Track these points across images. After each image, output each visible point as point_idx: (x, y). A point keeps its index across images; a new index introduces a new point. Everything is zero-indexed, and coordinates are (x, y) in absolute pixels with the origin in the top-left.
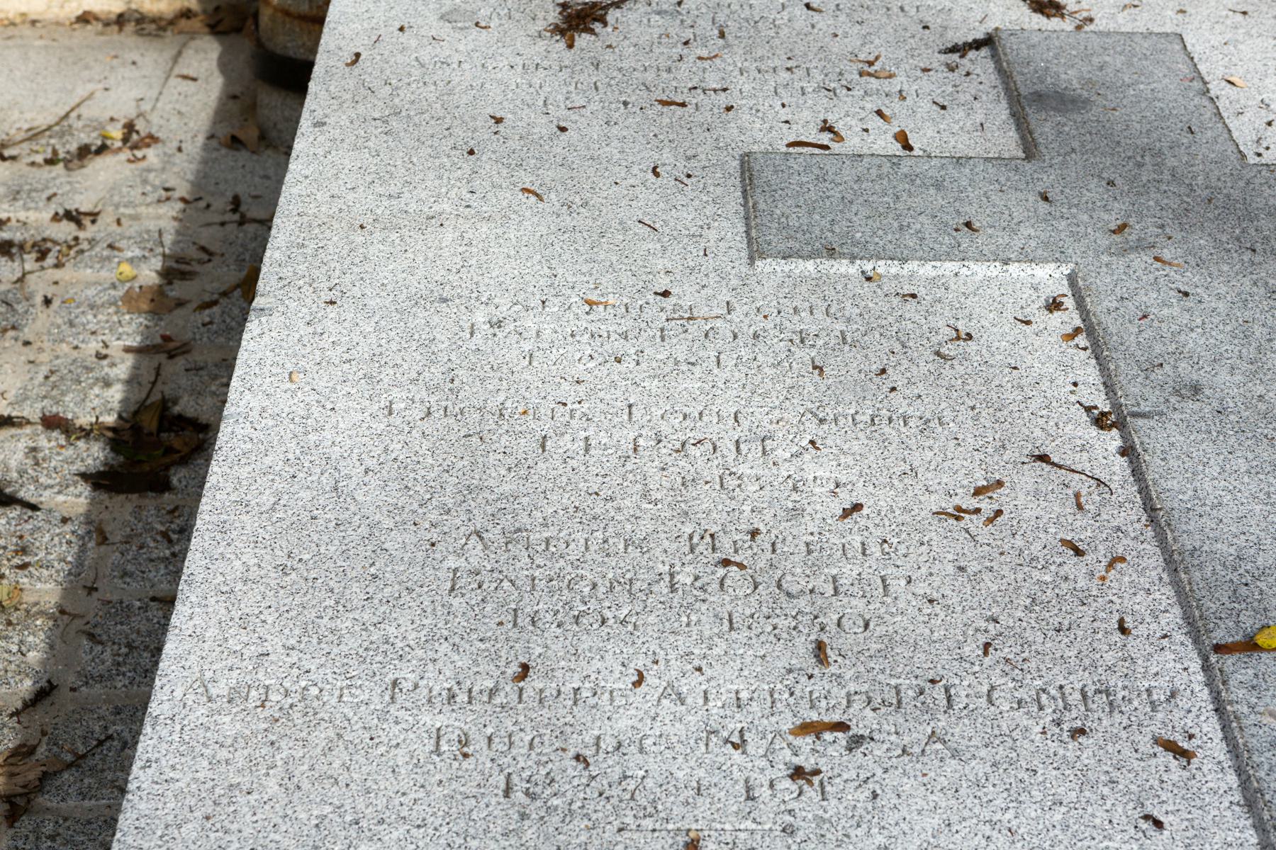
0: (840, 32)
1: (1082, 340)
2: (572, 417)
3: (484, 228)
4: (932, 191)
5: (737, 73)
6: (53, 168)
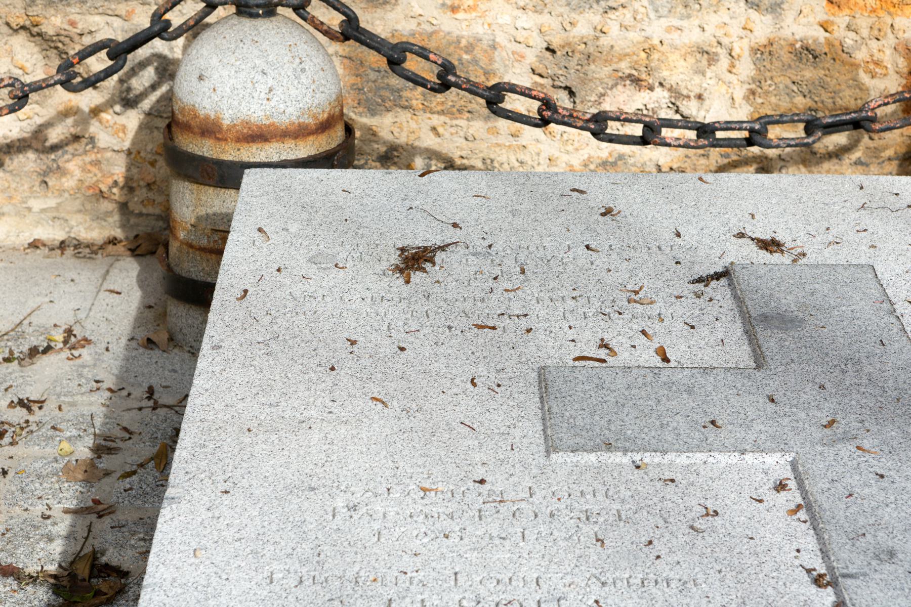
0: (612, 268)
1: (802, 515)
2: (411, 583)
3: (343, 430)
4: (685, 396)
5: (534, 301)
6: (9, 364)
